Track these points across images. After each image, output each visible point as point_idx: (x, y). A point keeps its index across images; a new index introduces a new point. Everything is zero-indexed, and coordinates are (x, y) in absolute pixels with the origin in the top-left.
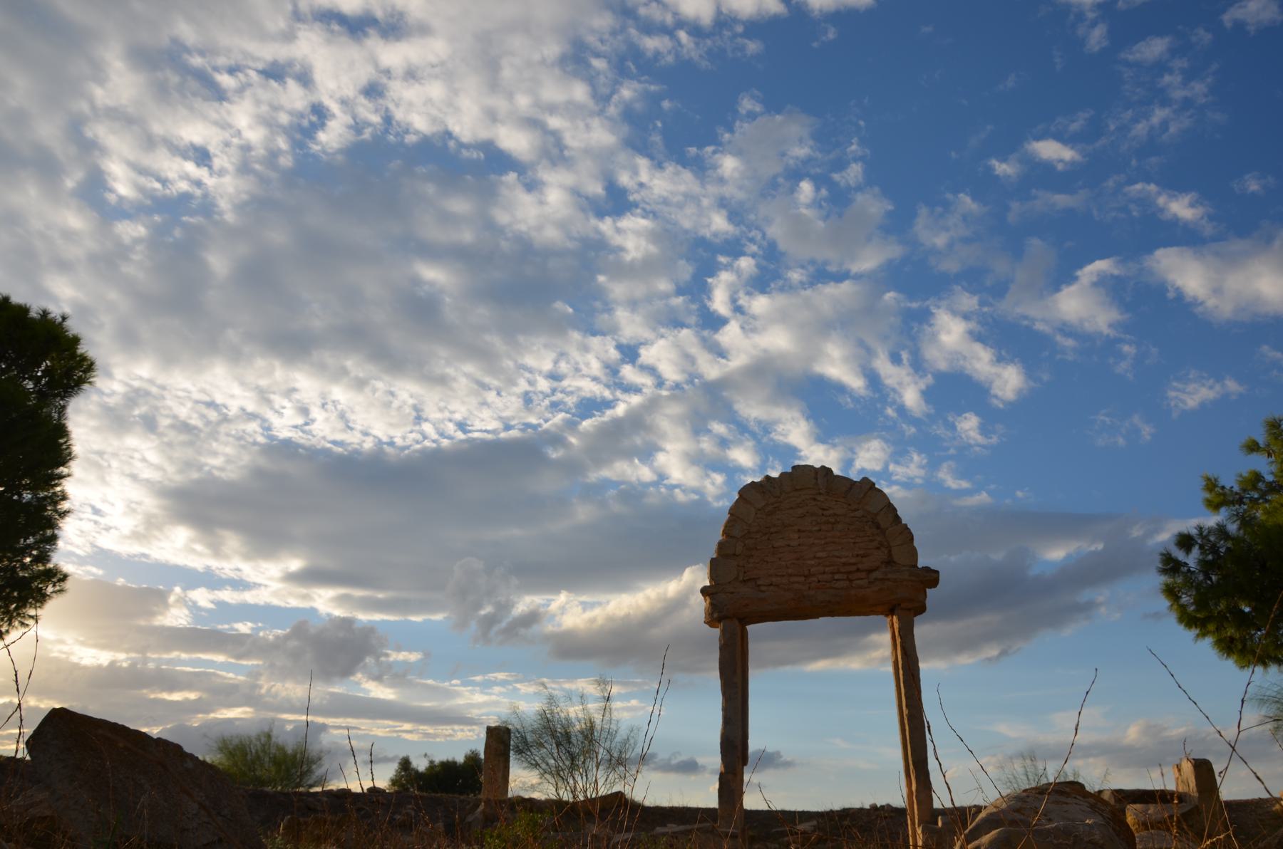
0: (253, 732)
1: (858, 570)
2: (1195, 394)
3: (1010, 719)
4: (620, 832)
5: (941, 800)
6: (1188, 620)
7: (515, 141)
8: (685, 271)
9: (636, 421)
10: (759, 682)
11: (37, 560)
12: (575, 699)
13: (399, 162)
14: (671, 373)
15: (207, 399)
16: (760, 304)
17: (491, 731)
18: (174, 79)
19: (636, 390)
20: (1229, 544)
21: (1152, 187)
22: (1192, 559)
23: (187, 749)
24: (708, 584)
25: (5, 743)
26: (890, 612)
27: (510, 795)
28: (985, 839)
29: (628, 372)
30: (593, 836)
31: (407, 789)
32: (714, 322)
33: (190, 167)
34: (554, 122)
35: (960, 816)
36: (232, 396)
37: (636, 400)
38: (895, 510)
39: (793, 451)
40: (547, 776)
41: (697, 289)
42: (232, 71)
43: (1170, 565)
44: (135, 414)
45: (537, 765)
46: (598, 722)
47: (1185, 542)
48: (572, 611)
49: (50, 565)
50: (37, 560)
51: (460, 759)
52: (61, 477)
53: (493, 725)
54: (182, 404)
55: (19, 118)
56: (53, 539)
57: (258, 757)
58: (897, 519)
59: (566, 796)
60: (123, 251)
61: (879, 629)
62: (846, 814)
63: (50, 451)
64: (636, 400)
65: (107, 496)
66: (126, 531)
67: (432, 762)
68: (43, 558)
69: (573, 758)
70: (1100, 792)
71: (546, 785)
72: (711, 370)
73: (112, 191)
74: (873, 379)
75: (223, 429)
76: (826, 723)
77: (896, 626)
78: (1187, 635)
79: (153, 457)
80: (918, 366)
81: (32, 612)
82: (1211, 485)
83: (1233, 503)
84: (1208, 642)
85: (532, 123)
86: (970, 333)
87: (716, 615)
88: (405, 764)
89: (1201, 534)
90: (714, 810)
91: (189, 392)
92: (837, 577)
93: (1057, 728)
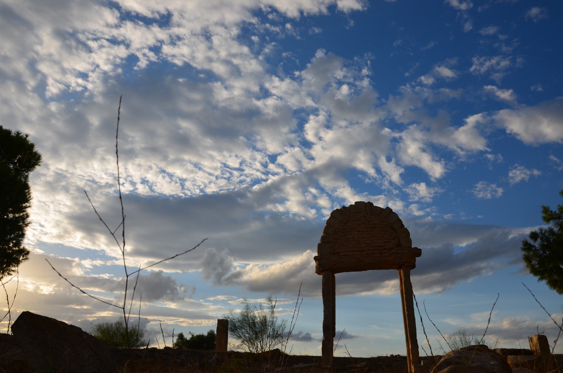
0: (114, 322)
1: (385, 249)
2: (518, 175)
3: (453, 317)
4: (280, 367)
5: (422, 354)
6: (535, 272)
7: (219, 69)
8: (294, 123)
9: (276, 187)
10: (340, 300)
11: (15, 245)
12: (258, 307)
13: (170, 77)
14: (291, 167)
15: (92, 179)
16: (328, 136)
17: (219, 321)
18: (73, 43)
19: (274, 174)
20: (555, 237)
21: (494, 87)
22: (537, 244)
23: (84, 330)
24: (317, 255)
25: (3, 328)
26: (399, 268)
27: (229, 350)
28: (445, 370)
29: (271, 167)
30: (266, 369)
31: (182, 348)
32: (306, 145)
33: (80, 81)
34: (236, 61)
35: (432, 360)
36: (103, 178)
37: (276, 178)
38: (401, 222)
39: (344, 200)
40: (245, 342)
41: (300, 128)
42: (96, 39)
43: (527, 247)
44: (58, 184)
45: (240, 337)
46: (268, 318)
47: (534, 236)
48: (255, 270)
49: (22, 247)
50: (15, 245)
51: (206, 334)
52: (26, 207)
53: (221, 318)
54: (81, 181)
55: (5, 59)
56: (23, 235)
57: (115, 334)
58: (403, 226)
59: (254, 351)
60: (52, 115)
61: (390, 278)
62: (380, 359)
63: (22, 196)
64: (276, 178)
65: (45, 215)
66: (54, 234)
67: (193, 336)
68: (18, 244)
69: (256, 333)
70: (495, 350)
71: (244, 346)
72: (308, 165)
73: (49, 91)
74: (378, 170)
75: (99, 191)
76: (370, 318)
77: (402, 274)
78: (533, 279)
79: (69, 203)
80: (398, 164)
81: (13, 269)
82: (546, 210)
83: (556, 219)
84: (544, 282)
85: (227, 62)
86: (420, 148)
87: (319, 270)
88: (181, 336)
89: (541, 232)
90: (320, 357)
91: (84, 176)
92: (375, 252)
93: (477, 321)
